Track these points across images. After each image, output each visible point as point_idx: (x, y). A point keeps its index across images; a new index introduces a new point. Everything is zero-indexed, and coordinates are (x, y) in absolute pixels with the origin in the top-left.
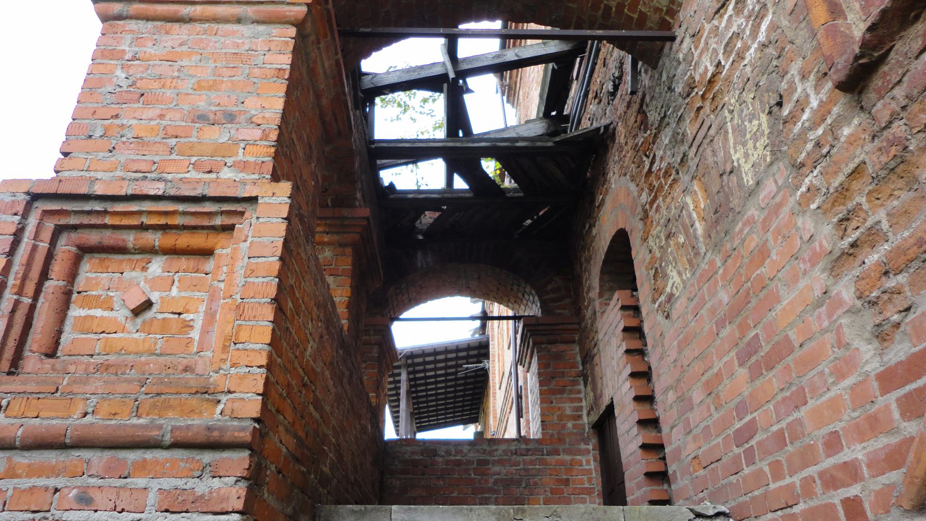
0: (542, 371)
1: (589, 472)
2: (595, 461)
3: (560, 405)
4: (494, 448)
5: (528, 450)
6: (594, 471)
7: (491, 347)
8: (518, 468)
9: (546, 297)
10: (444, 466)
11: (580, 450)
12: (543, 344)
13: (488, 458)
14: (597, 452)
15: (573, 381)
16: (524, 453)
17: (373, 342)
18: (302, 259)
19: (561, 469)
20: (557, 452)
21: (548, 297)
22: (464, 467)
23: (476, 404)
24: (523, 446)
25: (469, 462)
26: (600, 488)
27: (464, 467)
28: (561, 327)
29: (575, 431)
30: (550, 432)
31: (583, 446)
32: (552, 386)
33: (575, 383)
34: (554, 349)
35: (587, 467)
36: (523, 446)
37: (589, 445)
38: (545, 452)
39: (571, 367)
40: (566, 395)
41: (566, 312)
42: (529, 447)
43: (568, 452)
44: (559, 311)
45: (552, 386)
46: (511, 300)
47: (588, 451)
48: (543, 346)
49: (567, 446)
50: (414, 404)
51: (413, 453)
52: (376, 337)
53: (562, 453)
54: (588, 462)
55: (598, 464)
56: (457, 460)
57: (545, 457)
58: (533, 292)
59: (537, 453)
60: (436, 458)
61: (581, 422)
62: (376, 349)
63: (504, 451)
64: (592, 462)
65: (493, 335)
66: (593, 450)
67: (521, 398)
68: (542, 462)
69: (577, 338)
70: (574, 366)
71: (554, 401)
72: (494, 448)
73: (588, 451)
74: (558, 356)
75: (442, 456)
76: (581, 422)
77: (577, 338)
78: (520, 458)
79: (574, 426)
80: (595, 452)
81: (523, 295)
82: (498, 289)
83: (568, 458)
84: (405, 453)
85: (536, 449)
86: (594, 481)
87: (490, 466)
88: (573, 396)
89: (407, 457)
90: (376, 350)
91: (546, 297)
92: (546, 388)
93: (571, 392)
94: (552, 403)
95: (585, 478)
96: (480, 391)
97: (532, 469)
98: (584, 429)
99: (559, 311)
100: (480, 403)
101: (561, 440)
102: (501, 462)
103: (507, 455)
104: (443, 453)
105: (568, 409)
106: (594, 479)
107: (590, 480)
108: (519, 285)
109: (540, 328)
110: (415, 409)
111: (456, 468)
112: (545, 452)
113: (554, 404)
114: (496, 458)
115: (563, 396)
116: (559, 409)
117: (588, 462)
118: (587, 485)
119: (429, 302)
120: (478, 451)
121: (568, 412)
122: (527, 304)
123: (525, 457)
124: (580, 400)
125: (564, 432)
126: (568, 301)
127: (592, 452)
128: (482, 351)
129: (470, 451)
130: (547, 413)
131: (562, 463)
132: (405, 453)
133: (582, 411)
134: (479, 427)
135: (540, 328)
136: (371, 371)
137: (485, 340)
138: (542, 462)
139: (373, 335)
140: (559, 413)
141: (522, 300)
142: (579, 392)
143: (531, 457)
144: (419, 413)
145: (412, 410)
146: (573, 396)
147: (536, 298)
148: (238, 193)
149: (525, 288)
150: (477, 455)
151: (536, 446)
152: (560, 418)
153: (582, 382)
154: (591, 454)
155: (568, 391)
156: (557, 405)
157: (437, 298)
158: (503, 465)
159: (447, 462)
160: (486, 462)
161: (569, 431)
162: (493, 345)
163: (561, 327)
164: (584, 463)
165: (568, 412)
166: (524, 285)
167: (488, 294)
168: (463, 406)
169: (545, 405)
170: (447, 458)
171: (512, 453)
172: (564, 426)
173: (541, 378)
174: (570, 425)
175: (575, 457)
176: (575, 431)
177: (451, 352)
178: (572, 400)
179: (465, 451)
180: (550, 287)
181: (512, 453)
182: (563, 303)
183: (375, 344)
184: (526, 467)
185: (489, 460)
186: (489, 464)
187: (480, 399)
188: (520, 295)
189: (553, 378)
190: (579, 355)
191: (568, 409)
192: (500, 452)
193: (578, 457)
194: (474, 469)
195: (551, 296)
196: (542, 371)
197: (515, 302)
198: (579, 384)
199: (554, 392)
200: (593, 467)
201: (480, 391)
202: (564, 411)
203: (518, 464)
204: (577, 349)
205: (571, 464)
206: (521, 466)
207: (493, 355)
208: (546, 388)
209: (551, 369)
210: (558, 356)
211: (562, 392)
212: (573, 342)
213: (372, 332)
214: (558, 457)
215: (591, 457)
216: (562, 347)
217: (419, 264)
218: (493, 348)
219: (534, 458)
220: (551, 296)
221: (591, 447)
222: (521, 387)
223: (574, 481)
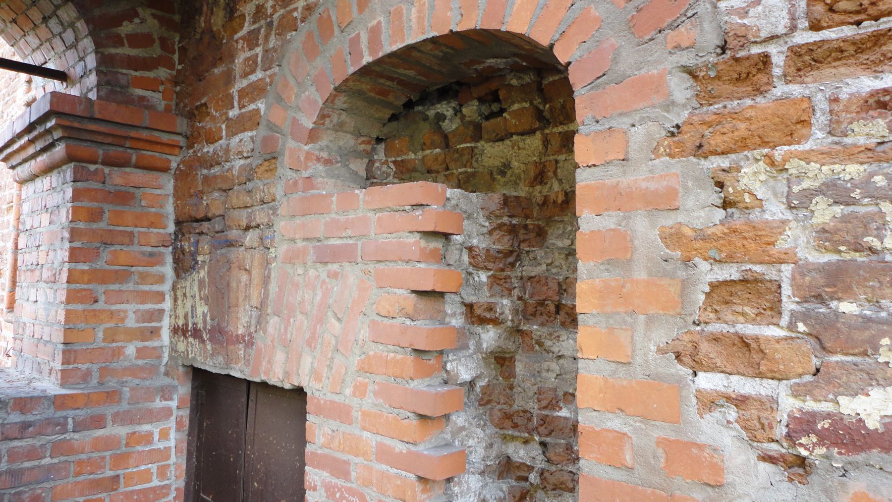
0: (81, 225)
1: (164, 454)
2: (178, 430)
3: (114, 307)
5: (25, 426)
9: (113, 51)
11: (150, 412)
12: (95, 163)
14: (186, 413)
15: (151, 255)
18: (419, 11)
26: (181, 483)
28: (145, 134)
29: (140, 362)
30: (84, 367)
33: (154, 259)
34: (117, 177)
35: (161, 446)
37: (171, 399)
38: (70, 426)
39: (152, 225)
40: (130, 286)
42: (30, 418)
43: (122, 418)
44: (139, 92)
47: (168, 412)
48: (92, 167)
49: (125, 406)
54: (164, 435)
55: (184, 436)
61: (155, 343)
64: (173, 435)
66: (178, 407)
68: (58, 449)
69: (174, 165)
70: (157, 222)
71: (102, 298)
73: (168, 412)
76: (155, 343)
77: (174, 165)
79: (141, 353)
83: (122, 431)
85: (50, 422)
86: (172, 472)
88: (147, 288)
92: (85, 267)
95: (154, 468)
97: (33, 468)
98: (160, 357)
99: (139, 92)
101: (112, 396)
105: (131, 315)
106: (172, 468)
107: (162, 473)
109: (93, 127)
115: (124, 287)
116: (112, 314)
117: (164, 435)
118: (155, 483)
124: (161, 297)
125: (114, 365)
126: (163, 73)
127: (175, 413)
133: (160, 320)
135: (93, 127)
140: (111, 325)
142: (161, 279)
143: (30, 441)
146: (147, 288)
148: (742, 382)
152: (111, 336)
153: (169, 259)
154: (173, 418)
155: (136, 277)
156: (107, 307)
161: (126, 364)
172: (117, 353)
174: (131, 350)
176: (140, 362)
178: (144, 297)
180: (126, 28)
182: (151, 74)
184: (16, 466)
190: (171, 200)
193: (146, 428)
195: (126, 51)
196: (81, 225)
197: (14, 21)
198: (162, 263)
199: (103, 277)
200: (172, 443)
202: (122, 320)
205: (127, 445)
208: (85, 267)
210: (123, 197)
211: (121, 277)
212: (165, 170)
214: (100, 433)
215: (172, 423)
216: (137, 176)
220: (126, 51)
221: (174, 404)
223: (129, 478)
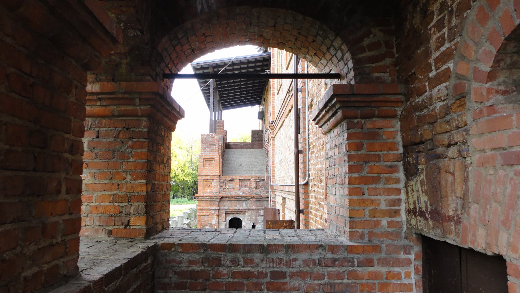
0: (353, 153)
3: (373, 198)
4: (293, 256)
5: (335, 260)
6: (414, 286)
7: (272, 62)
8: (322, 282)
9: (361, 56)
10: (230, 280)
11: (398, 260)
12: (357, 118)
13: (284, 269)
14: (420, 263)
15: (391, 167)
16: (330, 264)
17: (140, 114)
19: (374, 284)
20: (369, 263)
21: (364, 55)
22: (254, 280)
23: (260, 94)
24: (329, 255)
25: (263, 275)
27: (254, 280)
28: (381, 98)
29: (390, 230)
30: (360, 231)
31: (403, 256)
32: (364, 173)
33: (393, 169)
34: (369, 124)
35: (407, 282)
36: (329, 255)
37: (410, 254)
38: (356, 263)
39: (390, 149)
41: (386, 76)
42: (336, 256)
43: (383, 262)
45: (364, 173)
46: (310, 52)
48: (356, 121)
49: (383, 255)
50: (220, 95)
51: (191, 262)
52: (143, 107)
53: (376, 264)
54: (408, 275)
55: (420, 277)
56: (245, 272)
57: (355, 269)
58: (344, 47)
59: (346, 264)
60: (221, 269)
62: (144, 122)
63: (305, 261)
64: (413, 276)
65: (273, 54)
67: (299, 118)
68: (352, 275)
69: (399, 113)
71: (367, 192)
72: (293, 256)
73: (408, 262)
74: (373, 135)
75: (228, 267)
76: (398, 219)
77: (399, 113)
78: (326, 270)
80: (417, 263)
81: (328, 49)
82: (296, 39)
83: (383, 270)
84: (180, 263)
85: (345, 259)
87: (288, 280)
88: (390, 186)
89: (184, 267)
90: (144, 123)
91: (361, 56)
93: (388, 180)
94: (364, 194)
96: (264, 83)
97: (340, 284)
98: (401, 227)
99: (376, 75)
100: (262, 94)
102: (301, 275)
103: (309, 266)
104: (228, 263)
105: (383, 202)
108: (325, 37)
109: (353, 99)
110: (220, 98)
111: (245, 282)
112: (356, 263)
113: (366, 196)
114: (295, 270)
116: (372, 202)
117: (408, 275)
119: (216, 51)
120: (273, 261)
121: (383, 206)
122: (331, 59)
123: (331, 269)
124: (398, 191)
126: (388, 61)
128: (265, 63)
129: (263, 260)
130: (357, 208)
131: (376, 276)
132: (180, 263)
133: (399, 205)
134: (261, 107)
135: (353, 99)
136: (139, 151)
137: (268, 56)
138: (352, 275)
139: (140, 105)
141: (324, 54)
142: (398, 181)
144: (224, 100)
145: (218, 99)
146: (390, 186)
147: (348, 55)
149: (333, 41)
150: (271, 265)
151: (345, 255)
152: (373, 213)
155: (383, 180)
156: (370, 197)
157: (225, 46)
158: (303, 279)
159: (234, 274)
160: (282, 275)
161: (383, 230)
162: (273, 61)
163: (381, 98)
164: (403, 276)
165: (383, 206)
166: (332, 38)
167: (284, 44)
168: (252, 96)
169: (355, 197)
170: (233, 269)
171: (315, 263)
172: (377, 224)
173: (352, 163)
174: (384, 222)
175: (392, 269)
176: (390, 230)
177: (243, 63)
178: (389, 192)
179: (256, 261)
180: (366, 42)
181: (315, 263)
182: (381, 64)
183: (142, 116)
184: (332, 281)
185: (285, 273)
186: (286, 278)
187: (262, 91)
188: (324, 49)
189: (366, 162)
190: (399, 134)
191: (383, 202)
192: (299, 262)
193: (396, 269)
194: (267, 283)
196: (353, 153)
197: (315, 55)
198: (398, 171)
199: (366, 181)
200: (413, 281)
201: (264, 83)
202: (378, 205)
203: (321, 277)
204: (398, 125)
205: (387, 278)
206: (326, 280)
207: (273, 68)
209: (363, 152)
210: (373, 135)
211: (376, 180)
212: (394, 116)
213: (138, 102)
214: (371, 269)
215: (412, 269)
216: (379, 122)
217: (199, 7)
218: (273, 63)
219: (341, 270)
220: (368, 54)
221: (412, 257)
222: (300, 109)
